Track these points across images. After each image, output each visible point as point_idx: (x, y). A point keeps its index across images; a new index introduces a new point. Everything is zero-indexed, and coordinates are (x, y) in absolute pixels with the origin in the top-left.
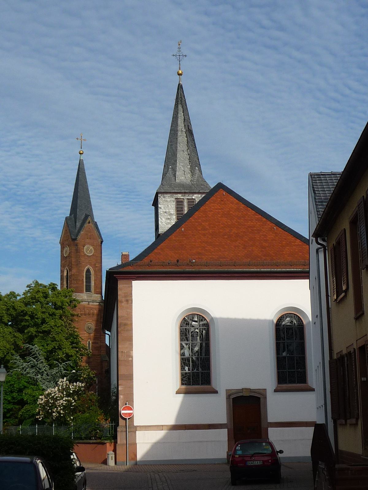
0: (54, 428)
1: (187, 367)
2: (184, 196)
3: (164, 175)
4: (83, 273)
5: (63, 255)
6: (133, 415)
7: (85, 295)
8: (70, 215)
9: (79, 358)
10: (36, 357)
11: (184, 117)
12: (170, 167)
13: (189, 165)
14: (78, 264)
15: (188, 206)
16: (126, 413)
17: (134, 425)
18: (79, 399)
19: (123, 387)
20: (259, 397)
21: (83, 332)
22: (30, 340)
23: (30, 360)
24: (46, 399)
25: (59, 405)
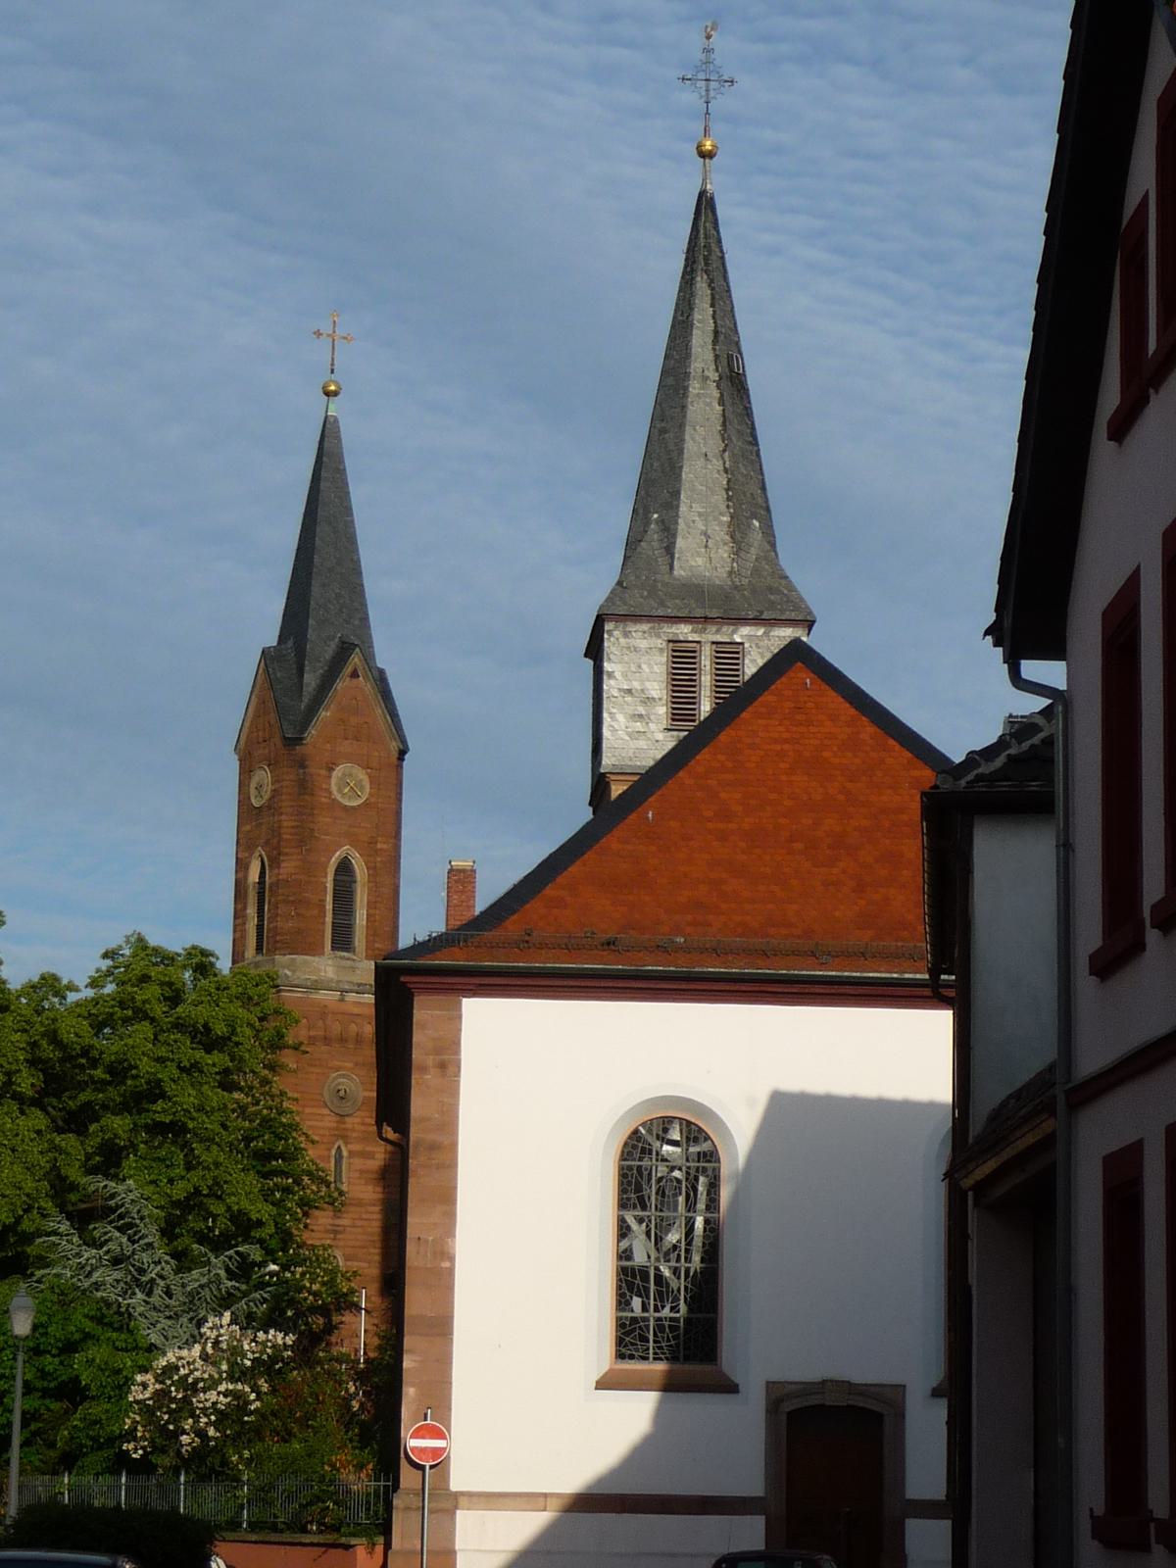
0: (182, 1487)
1: (640, 1300)
2: (703, 631)
3: (632, 544)
4: (326, 877)
5: (249, 798)
6: (448, 1457)
7: (330, 962)
8: (282, 639)
9: (293, 1215)
10: (131, 1226)
11: (715, 323)
12: (656, 516)
13: (726, 510)
14: (305, 838)
15: (717, 669)
16: (423, 1446)
17: (448, 1489)
18: (274, 1391)
19: (418, 1358)
20: (878, 1409)
21: (315, 1110)
22: (109, 1159)
23: (106, 1237)
24: (158, 1386)
25: (206, 1409)
